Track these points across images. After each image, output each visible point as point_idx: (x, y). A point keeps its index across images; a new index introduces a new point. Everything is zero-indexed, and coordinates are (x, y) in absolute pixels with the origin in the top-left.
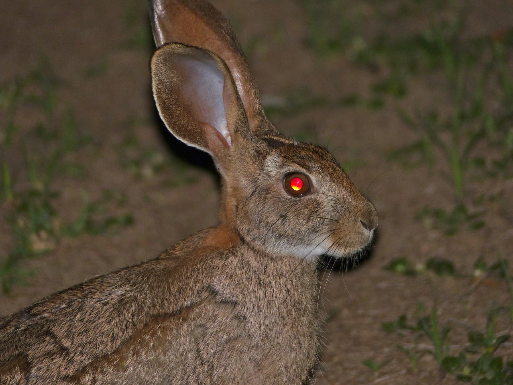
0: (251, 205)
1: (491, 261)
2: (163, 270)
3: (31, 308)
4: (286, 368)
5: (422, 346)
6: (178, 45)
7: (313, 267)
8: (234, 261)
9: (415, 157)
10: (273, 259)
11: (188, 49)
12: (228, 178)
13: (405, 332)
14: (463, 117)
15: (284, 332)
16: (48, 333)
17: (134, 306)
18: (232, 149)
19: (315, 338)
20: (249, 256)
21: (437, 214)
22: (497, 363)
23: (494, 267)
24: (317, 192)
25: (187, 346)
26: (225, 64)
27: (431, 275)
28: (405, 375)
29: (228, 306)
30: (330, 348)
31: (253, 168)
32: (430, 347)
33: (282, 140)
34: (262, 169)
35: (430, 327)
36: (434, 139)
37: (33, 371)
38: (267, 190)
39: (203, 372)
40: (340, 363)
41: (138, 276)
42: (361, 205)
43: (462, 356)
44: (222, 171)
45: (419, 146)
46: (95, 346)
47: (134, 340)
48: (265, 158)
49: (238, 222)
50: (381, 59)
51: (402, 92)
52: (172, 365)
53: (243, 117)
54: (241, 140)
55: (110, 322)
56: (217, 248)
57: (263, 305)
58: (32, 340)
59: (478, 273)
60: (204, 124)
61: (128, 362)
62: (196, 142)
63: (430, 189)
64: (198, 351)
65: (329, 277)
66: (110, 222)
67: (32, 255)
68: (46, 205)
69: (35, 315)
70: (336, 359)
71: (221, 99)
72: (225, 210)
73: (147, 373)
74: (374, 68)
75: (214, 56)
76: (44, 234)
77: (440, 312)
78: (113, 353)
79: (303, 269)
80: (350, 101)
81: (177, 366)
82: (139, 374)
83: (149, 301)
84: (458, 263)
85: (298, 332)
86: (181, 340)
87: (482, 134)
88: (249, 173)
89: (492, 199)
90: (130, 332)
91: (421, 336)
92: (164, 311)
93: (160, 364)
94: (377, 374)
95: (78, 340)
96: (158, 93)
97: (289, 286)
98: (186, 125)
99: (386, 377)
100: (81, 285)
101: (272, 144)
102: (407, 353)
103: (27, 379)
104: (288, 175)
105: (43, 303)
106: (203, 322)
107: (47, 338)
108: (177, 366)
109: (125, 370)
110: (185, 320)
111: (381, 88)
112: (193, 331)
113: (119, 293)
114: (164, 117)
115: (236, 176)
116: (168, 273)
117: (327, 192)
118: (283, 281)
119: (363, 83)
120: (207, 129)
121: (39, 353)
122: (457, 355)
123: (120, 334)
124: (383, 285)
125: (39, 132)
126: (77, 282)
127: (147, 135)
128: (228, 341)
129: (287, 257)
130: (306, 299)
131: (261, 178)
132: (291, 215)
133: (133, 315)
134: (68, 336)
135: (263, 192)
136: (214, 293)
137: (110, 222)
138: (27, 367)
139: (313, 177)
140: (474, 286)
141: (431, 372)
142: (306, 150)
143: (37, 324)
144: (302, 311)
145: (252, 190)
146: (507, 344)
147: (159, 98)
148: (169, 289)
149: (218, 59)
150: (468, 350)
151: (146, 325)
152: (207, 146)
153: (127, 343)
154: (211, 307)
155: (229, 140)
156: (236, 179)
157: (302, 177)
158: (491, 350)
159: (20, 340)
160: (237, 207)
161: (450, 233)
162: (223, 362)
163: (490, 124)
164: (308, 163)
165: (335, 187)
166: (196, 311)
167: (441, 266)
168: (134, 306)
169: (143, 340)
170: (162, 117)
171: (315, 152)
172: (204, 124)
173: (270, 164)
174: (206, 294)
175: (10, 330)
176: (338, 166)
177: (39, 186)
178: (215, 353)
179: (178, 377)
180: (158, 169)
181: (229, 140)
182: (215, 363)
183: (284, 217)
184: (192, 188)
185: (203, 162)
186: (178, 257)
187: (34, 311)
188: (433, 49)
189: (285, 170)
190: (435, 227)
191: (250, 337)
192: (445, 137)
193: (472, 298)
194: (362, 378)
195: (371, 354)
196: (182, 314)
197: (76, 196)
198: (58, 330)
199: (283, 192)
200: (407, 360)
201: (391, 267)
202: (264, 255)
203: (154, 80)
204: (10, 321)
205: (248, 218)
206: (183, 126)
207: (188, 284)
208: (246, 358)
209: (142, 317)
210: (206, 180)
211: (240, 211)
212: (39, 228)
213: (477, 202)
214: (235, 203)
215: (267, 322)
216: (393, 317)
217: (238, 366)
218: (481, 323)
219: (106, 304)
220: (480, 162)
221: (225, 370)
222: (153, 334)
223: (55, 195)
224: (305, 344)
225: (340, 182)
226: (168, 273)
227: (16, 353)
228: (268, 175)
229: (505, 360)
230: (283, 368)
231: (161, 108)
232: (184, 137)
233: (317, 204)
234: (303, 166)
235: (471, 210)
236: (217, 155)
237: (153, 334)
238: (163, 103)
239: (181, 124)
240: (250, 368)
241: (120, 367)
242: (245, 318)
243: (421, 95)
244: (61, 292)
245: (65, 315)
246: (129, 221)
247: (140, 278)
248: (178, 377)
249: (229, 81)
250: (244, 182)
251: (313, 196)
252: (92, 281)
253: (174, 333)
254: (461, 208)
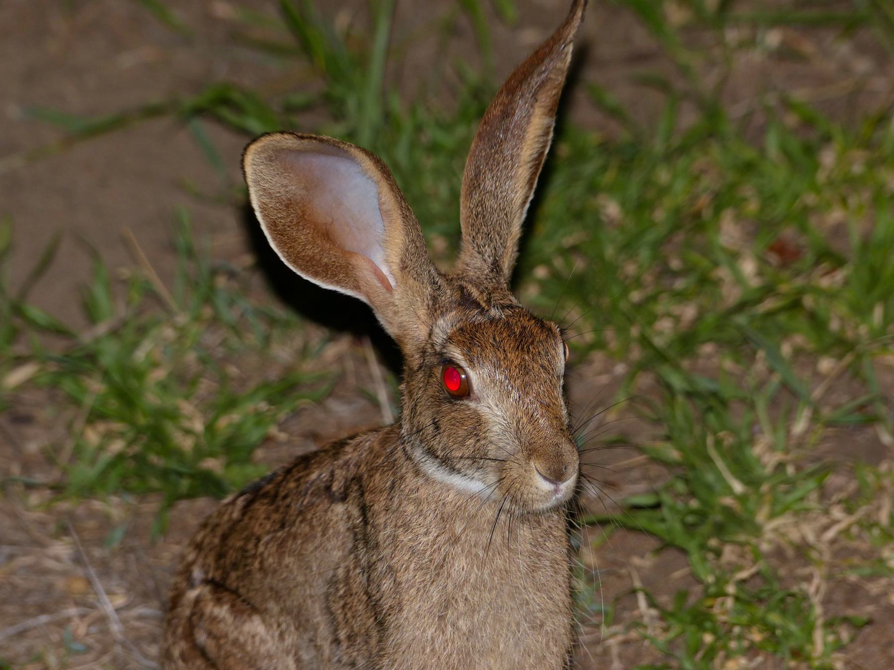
6: (286, 136)
11: (306, 142)
24: (478, 400)
54: (411, 281)
60: (352, 254)
62: (338, 283)
96: (263, 210)
98: (318, 257)
114: (277, 246)
120: (360, 263)
147: (265, 217)
152: (357, 288)
155: (392, 283)
172: (352, 254)
231: (271, 234)
232: (316, 274)
238: (273, 226)
239: (308, 256)
251: (472, 405)
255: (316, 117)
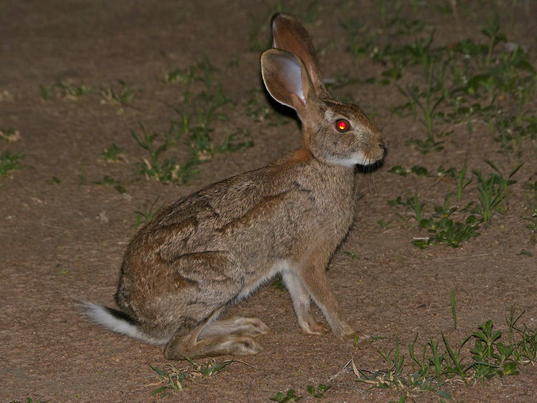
0: (318, 137)
1: (447, 168)
2: (271, 173)
3: (199, 192)
4: (336, 226)
5: (409, 213)
7: (352, 172)
8: (309, 168)
9: (406, 111)
10: (329, 167)
12: (305, 122)
13: (400, 206)
14: (432, 90)
15: (335, 207)
16: (208, 205)
17: (254, 192)
18: (307, 107)
19: (353, 209)
20: (317, 165)
21: (418, 142)
22: (450, 223)
23: (448, 171)
24: (353, 130)
25: (283, 214)
26: (302, 60)
27: (415, 175)
28: (400, 229)
29: (306, 192)
30: (360, 214)
31: (318, 117)
32: (414, 214)
33: (334, 102)
34: (323, 118)
35: (414, 203)
36: (417, 102)
37: (199, 226)
38: (326, 129)
39: (292, 228)
40: (365, 222)
41: (256, 176)
42: (377, 135)
43: (431, 219)
44: (301, 119)
45: (408, 105)
46: (233, 213)
47: (254, 210)
48: (325, 112)
49: (311, 146)
50: (387, 58)
51: (399, 76)
52: (274, 224)
53: (313, 88)
54: (311, 101)
55: (241, 200)
56: (299, 161)
57: (324, 192)
58: (199, 209)
59: (439, 174)
60: (292, 93)
61: (251, 222)
62: (287, 103)
63: (414, 129)
64: (289, 216)
65: (360, 176)
66: (241, 145)
67: (199, 163)
68: (207, 136)
69: (201, 196)
70: (363, 220)
71: (300, 80)
72: (303, 140)
73: (261, 228)
74: (384, 64)
75: (295, 56)
76: (205, 151)
77: (419, 195)
78: (243, 217)
79: (346, 172)
80: (371, 81)
81: (277, 224)
82: (256, 229)
83: (262, 189)
84: (429, 168)
85: (343, 207)
86: (280, 211)
87: (442, 99)
88: (316, 119)
89: (447, 134)
90: (252, 206)
91: (409, 208)
92: (270, 195)
93: (268, 223)
94: (385, 228)
95: (224, 210)
97: (338, 181)
99: (390, 230)
100: (226, 180)
101: (329, 104)
102: (401, 217)
103: (196, 230)
104: (337, 121)
105: (205, 189)
106: (292, 201)
107: (207, 208)
108: (277, 224)
109: (250, 226)
110: (282, 199)
111: (387, 74)
112: (286, 206)
113: (246, 184)
115: (310, 121)
116: (273, 174)
117: (359, 129)
118: (335, 178)
119: (379, 70)
120: (293, 96)
121: (202, 216)
122: (428, 219)
123: (247, 207)
124: (389, 180)
125: (203, 96)
126: (223, 179)
127: (260, 98)
128: (305, 211)
129: (337, 166)
130: (348, 188)
131: (323, 123)
132: (339, 142)
133: (254, 197)
134: (218, 207)
135: (324, 130)
136: (298, 185)
137: (241, 145)
138: (196, 224)
139: (351, 123)
140: (437, 181)
141: (414, 227)
142: (346, 107)
143: (202, 200)
144: (345, 195)
145: (318, 129)
146: (455, 213)
147: (265, 78)
148: (273, 183)
149: (297, 57)
150: (434, 216)
151: (261, 202)
152: (293, 105)
153: (250, 212)
154: (296, 193)
155: (305, 102)
156: (309, 123)
157: (346, 122)
158: (447, 216)
159: (192, 209)
160: (310, 138)
161: (425, 152)
162: (303, 223)
163: (446, 94)
164: (348, 114)
165: (363, 127)
166: (288, 195)
167: (420, 170)
168: (254, 192)
169: (259, 210)
170: (267, 89)
171: (352, 108)
172: (292, 93)
173: (327, 115)
174: (294, 186)
175: (187, 204)
176: (365, 115)
177: (203, 125)
178: (298, 218)
179: (278, 230)
180: (267, 117)
181: (305, 102)
182: (298, 223)
183: (335, 144)
184: (284, 128)
185: (291, 114)
186: (279, 166)
187: (200, 194)
188: (416, 53)
189: (336, 118)
190: (416, 149)
191: (317, 209)
192: (422, 100)
193: (436, 188)
194: (377, 230)
195: (382, 217)
196: (280, 196)
197: (224, 131)
198: (213, 204)
199: (335, 130)
200: (401, 221)
201: (393, 170)
202: (325, 164)
203: (262, 68)
204: (187, 199)
205: (316, 144)
206: (279, 93)
207: (283, 181)
208: (315, 221)
209: (259, 197)
210: (293, 123)
211: (312, 141)
212: (203, 148)
213: (439, 136)
214: (309, 136)
215: (326, 201)
216: (394, 198)
217: (311, 225)
218: (442, 200)
219: (239, 190)
220: (441, 114)
221: (304, 227)
222: (264, 207)
223: (211, 130)
224: (347, 213)
225: (365, 123)
226: (273, 174)
227: (190, 216)
228: (327, 121)
229: (454, 221)
230: (334, 226)
232: (280, 100)
233: (353, 136)
234: (346, 116)
235: (436, 140)
236: (298, 110)
237: (264, 207)
238: (268, 81)
240: (317, 225)
241: (247, 225)
242: (314, 199)
243: (409, 78)
244: (215, 184)
245: (217, 196)
246: (252, 145)
247: (258, 177)
248: (278, 230)
249: (304, 70)
250: (313, 124)
251: (351, 132)
252: (232, 178)
253: (276, 206)
254: (431, 139)
255: (294, 36)
